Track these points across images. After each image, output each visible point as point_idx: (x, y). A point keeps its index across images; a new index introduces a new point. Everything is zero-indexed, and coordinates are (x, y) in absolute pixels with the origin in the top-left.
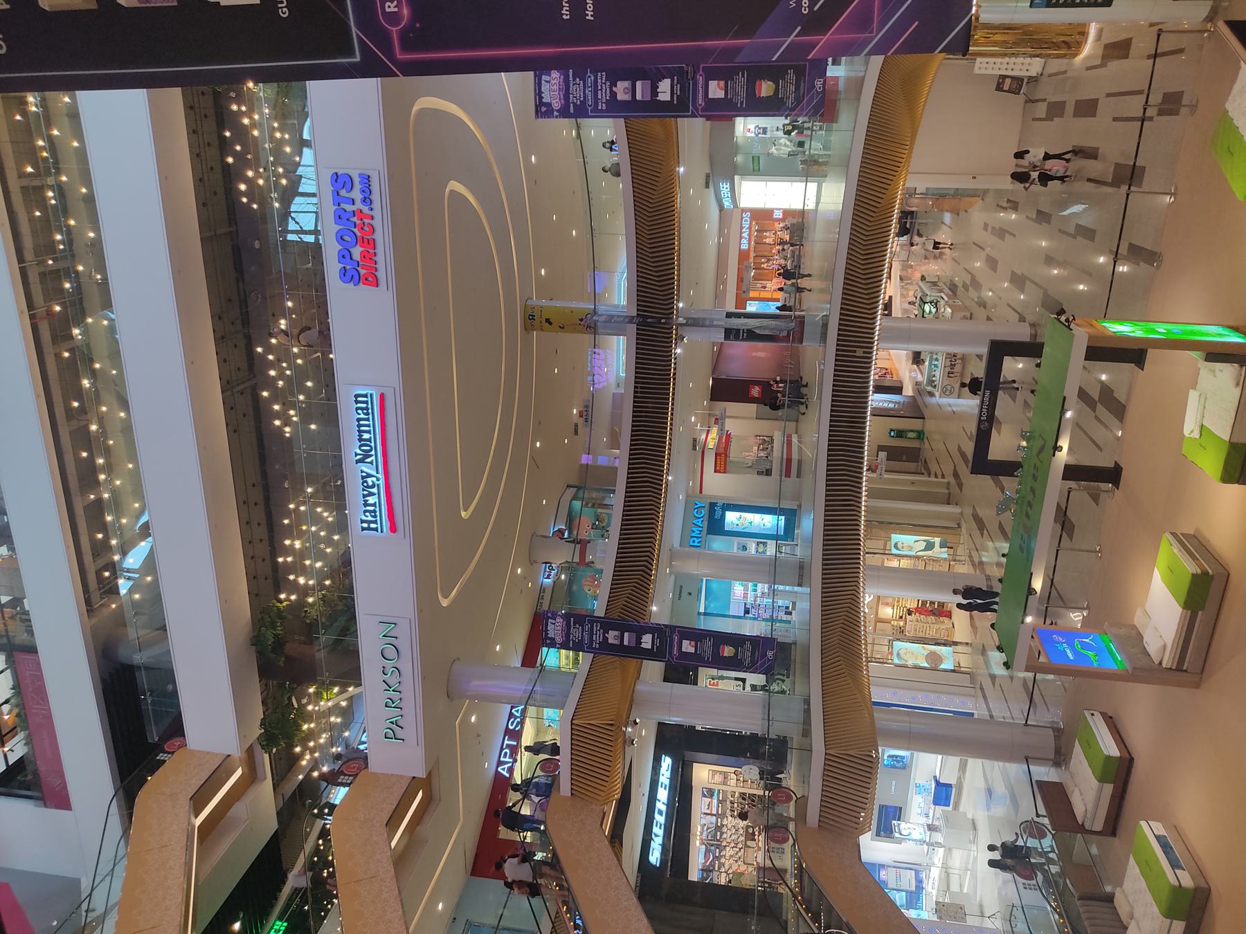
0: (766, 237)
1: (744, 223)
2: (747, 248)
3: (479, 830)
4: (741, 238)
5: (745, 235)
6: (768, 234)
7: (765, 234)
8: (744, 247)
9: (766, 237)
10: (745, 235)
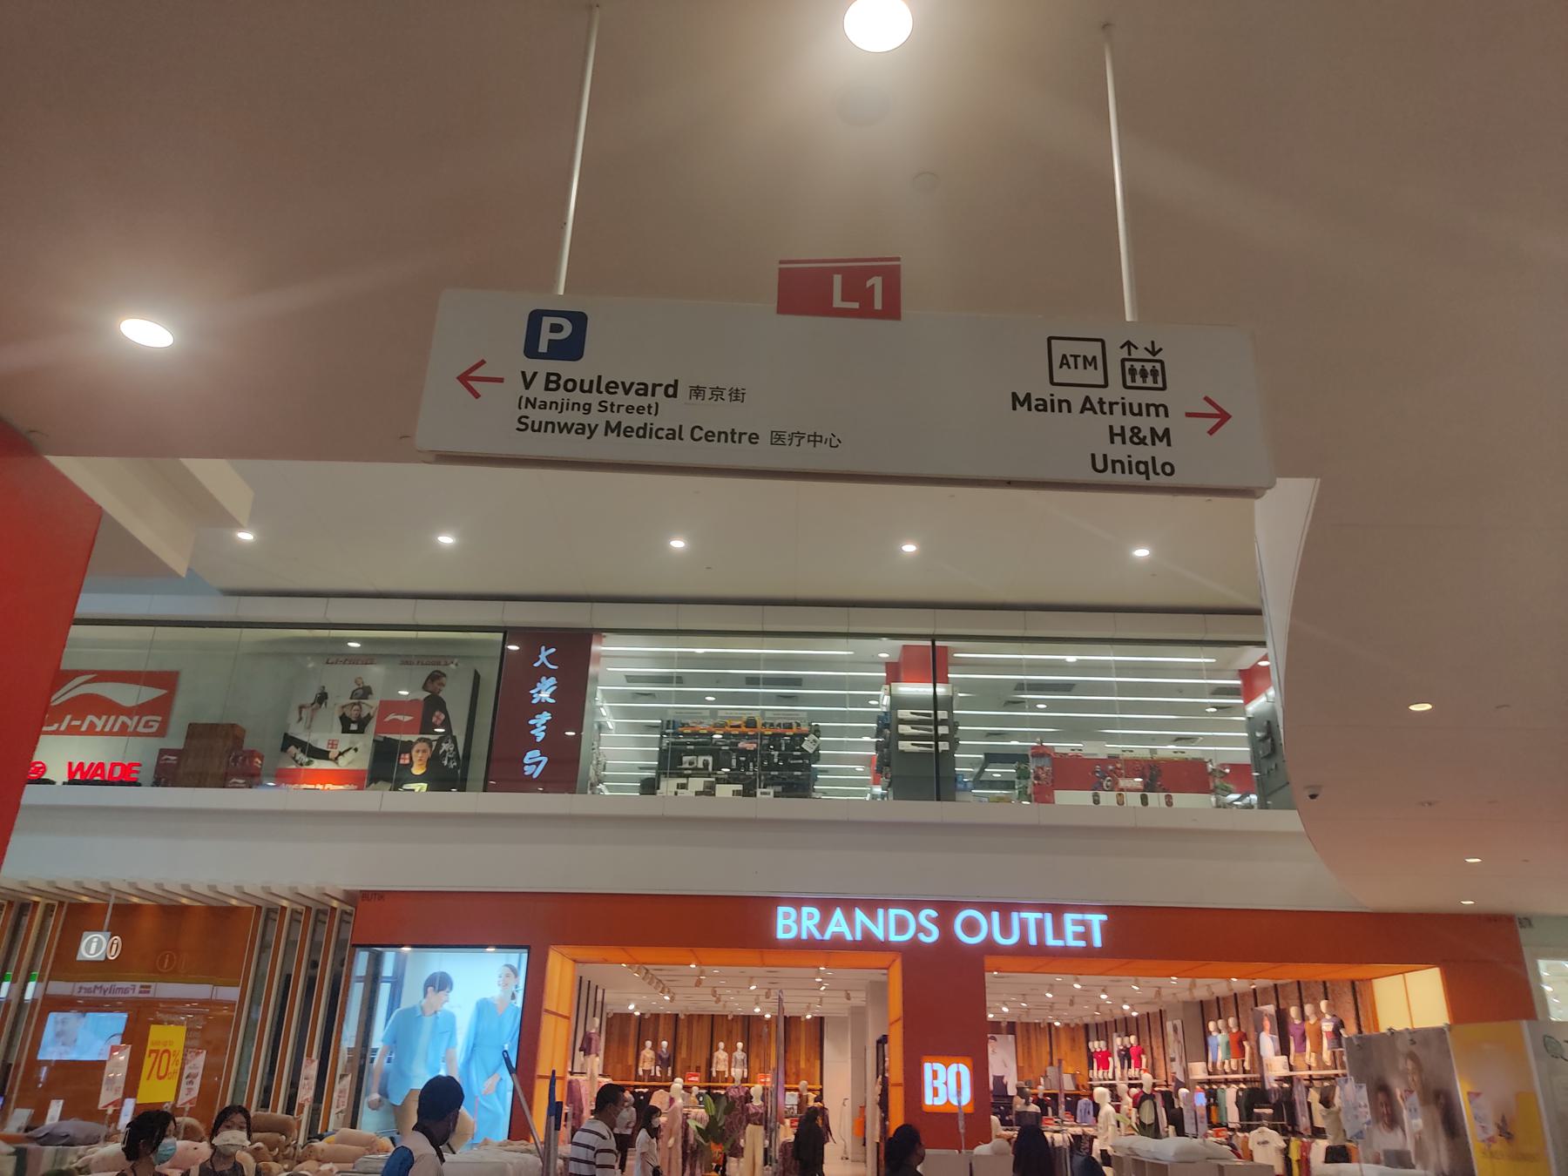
0: (730, 1050)
1: (893, 912)
2: (781, 935)
3: (1391, 911)
4: (826, 906)
5: (838, 924)
6: (739, 1055)
7: (740, 1045)
8: (781, 922)
9: (730, 1050)
10: (838, 924)
